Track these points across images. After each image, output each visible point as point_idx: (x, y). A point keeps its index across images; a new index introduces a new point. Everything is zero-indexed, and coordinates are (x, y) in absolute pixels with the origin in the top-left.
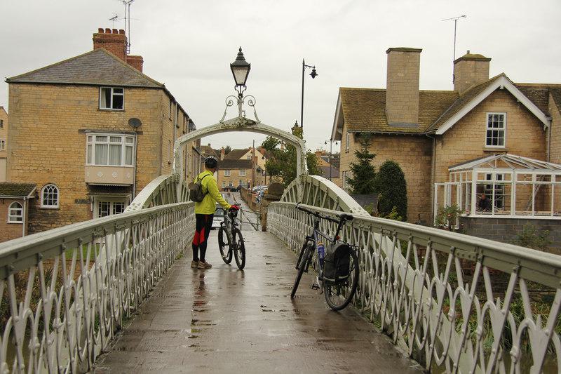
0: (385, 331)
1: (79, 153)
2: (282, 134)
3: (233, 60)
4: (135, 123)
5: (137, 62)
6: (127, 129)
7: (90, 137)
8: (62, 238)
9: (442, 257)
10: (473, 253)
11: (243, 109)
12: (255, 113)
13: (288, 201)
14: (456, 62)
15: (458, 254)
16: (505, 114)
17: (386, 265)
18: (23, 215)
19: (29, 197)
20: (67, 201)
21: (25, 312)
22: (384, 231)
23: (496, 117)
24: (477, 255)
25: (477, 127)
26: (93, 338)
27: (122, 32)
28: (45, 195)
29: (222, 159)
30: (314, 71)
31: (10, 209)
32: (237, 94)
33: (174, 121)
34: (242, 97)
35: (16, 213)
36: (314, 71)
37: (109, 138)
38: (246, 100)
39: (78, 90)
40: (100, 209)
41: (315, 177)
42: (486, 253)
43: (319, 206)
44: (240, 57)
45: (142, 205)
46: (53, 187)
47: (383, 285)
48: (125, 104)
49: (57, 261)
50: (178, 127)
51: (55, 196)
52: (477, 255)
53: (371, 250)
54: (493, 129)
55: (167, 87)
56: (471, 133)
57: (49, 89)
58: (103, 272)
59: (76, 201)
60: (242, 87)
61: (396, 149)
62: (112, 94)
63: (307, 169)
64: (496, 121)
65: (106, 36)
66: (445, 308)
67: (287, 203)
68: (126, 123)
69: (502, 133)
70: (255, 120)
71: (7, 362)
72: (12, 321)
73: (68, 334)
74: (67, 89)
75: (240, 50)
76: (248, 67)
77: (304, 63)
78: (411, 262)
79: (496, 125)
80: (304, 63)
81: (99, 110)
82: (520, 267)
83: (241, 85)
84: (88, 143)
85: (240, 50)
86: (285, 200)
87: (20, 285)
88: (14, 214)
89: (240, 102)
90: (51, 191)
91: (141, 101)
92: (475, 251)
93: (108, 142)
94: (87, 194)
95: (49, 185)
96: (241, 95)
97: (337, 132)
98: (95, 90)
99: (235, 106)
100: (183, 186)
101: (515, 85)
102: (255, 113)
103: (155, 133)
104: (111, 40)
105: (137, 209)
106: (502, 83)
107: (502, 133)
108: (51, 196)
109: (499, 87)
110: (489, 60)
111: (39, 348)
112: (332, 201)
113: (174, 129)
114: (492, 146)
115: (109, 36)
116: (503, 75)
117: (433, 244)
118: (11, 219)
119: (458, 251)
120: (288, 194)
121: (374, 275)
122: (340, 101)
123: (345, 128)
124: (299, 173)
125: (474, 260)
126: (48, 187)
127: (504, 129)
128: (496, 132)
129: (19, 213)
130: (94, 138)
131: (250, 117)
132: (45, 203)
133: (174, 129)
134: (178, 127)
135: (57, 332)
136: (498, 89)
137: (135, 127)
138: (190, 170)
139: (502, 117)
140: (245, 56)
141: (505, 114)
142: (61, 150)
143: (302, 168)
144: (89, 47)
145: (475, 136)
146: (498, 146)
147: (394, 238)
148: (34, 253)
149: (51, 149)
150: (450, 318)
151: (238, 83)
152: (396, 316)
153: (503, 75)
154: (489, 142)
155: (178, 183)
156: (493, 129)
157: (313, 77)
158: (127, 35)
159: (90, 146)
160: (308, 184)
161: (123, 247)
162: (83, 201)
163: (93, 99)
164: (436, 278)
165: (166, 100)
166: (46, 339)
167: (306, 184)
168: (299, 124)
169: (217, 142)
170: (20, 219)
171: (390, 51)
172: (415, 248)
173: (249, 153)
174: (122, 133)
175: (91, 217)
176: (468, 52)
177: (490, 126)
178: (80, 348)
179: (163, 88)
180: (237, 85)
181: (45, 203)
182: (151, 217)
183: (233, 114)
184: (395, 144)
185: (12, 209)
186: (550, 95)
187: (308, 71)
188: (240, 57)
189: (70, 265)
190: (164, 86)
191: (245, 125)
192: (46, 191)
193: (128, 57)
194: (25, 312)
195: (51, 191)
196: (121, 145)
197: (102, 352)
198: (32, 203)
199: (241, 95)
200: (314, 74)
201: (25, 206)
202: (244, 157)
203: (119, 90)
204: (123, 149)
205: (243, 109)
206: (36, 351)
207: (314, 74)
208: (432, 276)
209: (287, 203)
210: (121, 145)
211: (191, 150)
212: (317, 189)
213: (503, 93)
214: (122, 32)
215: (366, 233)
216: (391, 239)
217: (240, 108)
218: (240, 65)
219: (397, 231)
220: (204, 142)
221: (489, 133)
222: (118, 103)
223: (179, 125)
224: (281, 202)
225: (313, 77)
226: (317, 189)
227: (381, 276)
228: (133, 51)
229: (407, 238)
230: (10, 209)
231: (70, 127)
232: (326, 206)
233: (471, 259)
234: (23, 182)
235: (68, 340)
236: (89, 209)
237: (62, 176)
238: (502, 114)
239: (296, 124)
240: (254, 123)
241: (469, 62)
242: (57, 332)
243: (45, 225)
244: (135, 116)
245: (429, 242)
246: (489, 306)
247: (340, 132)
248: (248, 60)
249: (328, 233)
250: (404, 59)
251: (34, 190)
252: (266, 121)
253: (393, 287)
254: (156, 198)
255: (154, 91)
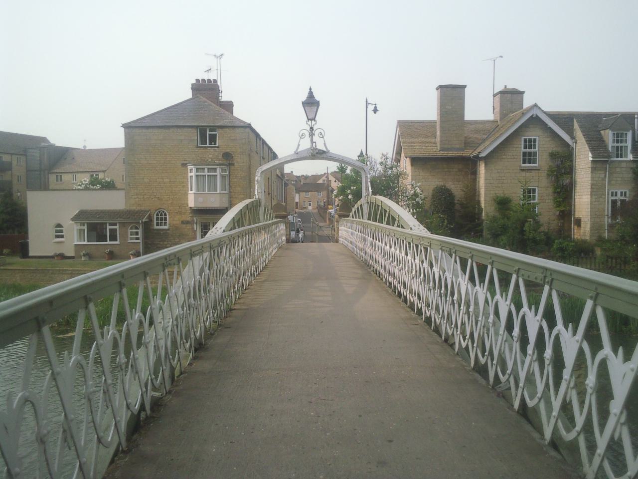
0: (446, 340)
1: (183, 183)
2: (345, 159)
3: (359, 154)
4: (227, 156)
5: (229, 106)
6: (220, 162)
7: (191, 170)
8: (122, 274)
9: (505, 279)
10: (540, 276)
11: (314, 141)
12: (325, 144)
13: (356, 218)
14: (495, 96)
15: (523, 275)
16: (537, 138)
17: (446, 279)
18: (140, 236)
19: (144, 221)
20: (175, 222)
21: (158, 301)
22: (443, 248)
23: (530, 141)
24: (545, 277)
25: (514, 149)
26: (170, 362)
27: (215, 81)
28: (157, 219)
29: (302, 183)
30: (376, 107)
31: (130, 231)
32: (308, 128)
33: (260, 154)
34: (313, 130)
35: (135, 234)
36: (376, 107)
37: (206, 170)
38: (317, 133)
39: (179, 131)
40: (202, 228)
41: (378, 197)
42: (554, 276)
43: (382, 223)
44: (311, 95)
45: (224, 228)
46: (163, 212)
47: (444, 298)
48: (218, 142)
49: (161, 276)
50: (263, 158)
51: (166, 219)
52: (545, 277)
53: (431, 265)
54: (528, 150)
55: (254, 126)
56: (511, 154)
57: (157, 131)
58: (179, 299)
59: (183, 222)
60: (313, 121)
61: (446, 170)
62: (208, 133)
63: (370, 190)
64: (530, 144)
65: (202, 85)
66: (509, 327)
67: (355, 219)
68: (220, 157)
69: (535, 153)
70: (325, 150)
71: (125, 354)
72: (127, 325)
73: (136, 368)
74: (171, 130)
75: (310, 89)
76: (317, 104)
77: (367, 101)
78: (472, 279)
79: (530, 147)
80: (367, 101)
81: (198, 147)
82: (597, 294)
83: (311, 120)
84: (190, 174)
85: (310, 89)
86: (353, 218)
87: (133, 296)
88: (133, 235)
89: (312, 135)
90: (161, 215)
91: (231, 138)
92: (543, 273)
93: (206, 173)
94: (191, 217)
95: (160, 210)
96: (312, 129)
97: (395, 157)
98: (194, 131)
99: (307, 139)
100: (265, 208)
101: (545, 113)
102: (325, 144)
103: (244, 164)
104: (206, 90)
105: (218, 233)
106: (535, 112)
107: (535, 153)
108: (162, 220)
109: (533, 115)
110: (523, 93)
111: (183, 314)
112: (394, 219)
113: (260, 161)
114: (527, 165)
115: (204, 85)
116: (536, 105)
117: (495, 263)
118: (131, 239)
119: (522, 272)
120: (358, 208)
121: (434, 288)
122: (398, 130)
123: (403, 154)
124: (364, 193)
125: (542, 282)
126: (159, 212)
127: (537, 149)
128: (530, 153)
129: (137, 233)
130: (194, 170)
131: (320, 146)
132: (158, 225)
133: (260, 161)
134: (263, 158)
135: (146, 347)
136: (532, 117)
137: (227, 160)
138: (275, 194)
139: (535, 140)
140: (314, 94)
141: (537, 138)
142: (169, 180)
143: (367, 189)
144: (188, 95)
145: (513, 157)
146: (532, 165)
147: (454, 255)
148: (143, 272)
149: (161, 180)
150: (514, 338)
151: (309, 118)
152: (457, 328)
153: (536, 105)
154: (524, 162)
155: (260, 206)
156: (528, 150)
157: (375, 113)
158: (219, 83)
159: (191, 176)
160: (372, 203)
161: (202, 271)
162: (187, 222)
163: (193, 138)
164: (498, 297)
165: (252, 136)
166: (133, 355)
167: (371, 204)
168: (364, 153)
169: (298, 169)
170: (138, 239)
171: (441, 87)
172: (474, 265)
173: (324, 178)
174: (218, 165)
175: (195, 238)
176: (506, 86)
177: (525, 148)
178: (195, 330)
179: (249, 126)
180: (309, 120)
181: (158, 225)
182: (231, 239)
183: (306, 144)
184: (445, 166)
185: (131, 230)
186: (575, 121)
187: (371, 108)
188: (311, 95)
189: (173, 278)
190: (250, 124)
191: (317, 154)
192: (157, 215)
193: (220, 102)
194: (158, 301)
195: (161, 215)
196: (216, 175)
197: (181, 373)
198: (147, 226)
199: (312, 129)
200: (375, 110)
201: (141, 227)
202: (321, 181)
203: (213, 128)
204: (218, 177)
205: (314, 141)
206: (182, 317)
207: (375, 110)
208: (493, 294)
209: (355, 219)
210: (216, 175)
211: (275, 177)
212: (380, 207)
213: (535, 121)
214: (215, 81)
215: (426, 249)
216: (451, 255)
217: (312, 140)
218: (311, 103)
219: (457, 248)
220: (288, 169)
221: (524, 154)
222: (213, 139)
223: (264, 157)
224: (350, 218)
225: (375, 113)
226: (380, 207)
227: (441, 290)
228: (224, 97)
229: (467, 256)
230: (130, 231)
231: (175, 162)
232: (388, 223)
233: (538, 281)
234: (139, 208)
235: (137, 372)
236: (193, 228)
237: (170, 202)
238: (534, 138)
239: (362, 152)
240: (324, 152)
241: (506, 95)
242: (146, 347)
243: (158, 242)
244: (228, 151)
245: (491, 261)
246: (559, 331)
247: (399, 158)
248: (317, 97)
249: (391, 247)
250: (452, 96)
251: (148, 214)
252: (334, 150)
253: (453, 301)
254: (237, 222)
255: (242, 129)
